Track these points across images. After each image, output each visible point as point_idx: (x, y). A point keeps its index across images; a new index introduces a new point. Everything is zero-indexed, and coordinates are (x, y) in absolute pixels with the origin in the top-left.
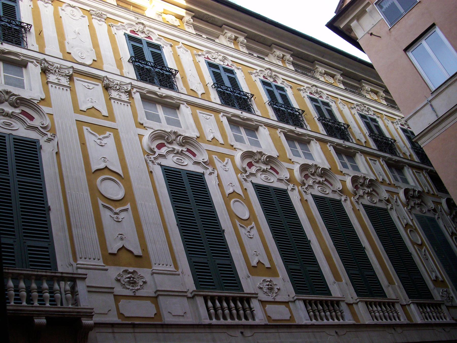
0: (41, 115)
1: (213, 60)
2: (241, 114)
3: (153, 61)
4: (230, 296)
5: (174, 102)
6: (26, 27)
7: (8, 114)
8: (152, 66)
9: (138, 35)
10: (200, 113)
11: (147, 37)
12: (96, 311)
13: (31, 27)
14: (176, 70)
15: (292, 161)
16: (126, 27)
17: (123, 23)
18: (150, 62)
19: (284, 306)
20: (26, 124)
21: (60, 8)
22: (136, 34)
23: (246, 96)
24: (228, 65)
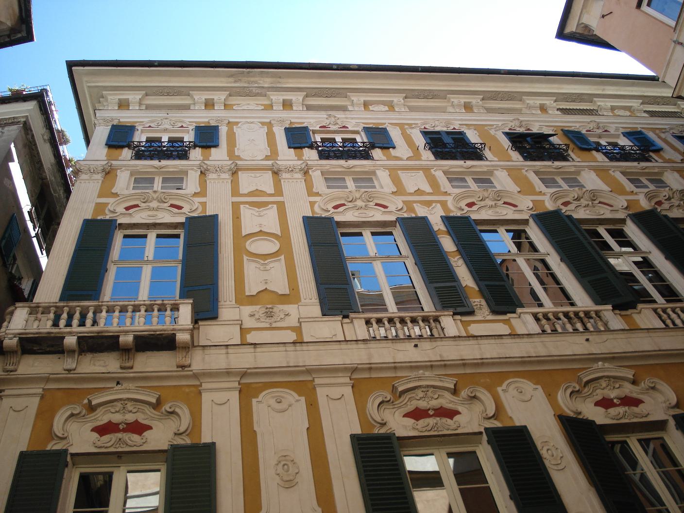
0: (389, 200)
1: (433, 128)
2: (638, 165)
3: (453, 142)
4: (430, 316)
5: (367, 170)
6: (480, 147)
7: (153, 208)
8: (452, 148)
9: (329, 128)
10: (402, 173)
11: (526, 130)
12: (611, 311)
13: (485, 146)
14: (566, 145)
15: (543, 192)
16: (315, 124)
17: (418, 124)
18: (448, 144)
19: (501, 324)
20: (173, 212)
21: (499, 389)
22: (327, 128)
23: (559, 149)
24: (454, 129)
